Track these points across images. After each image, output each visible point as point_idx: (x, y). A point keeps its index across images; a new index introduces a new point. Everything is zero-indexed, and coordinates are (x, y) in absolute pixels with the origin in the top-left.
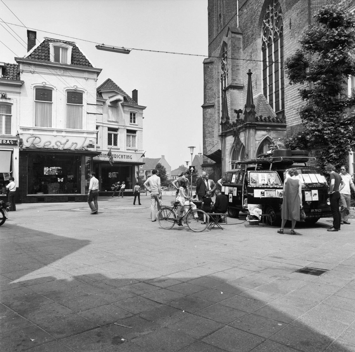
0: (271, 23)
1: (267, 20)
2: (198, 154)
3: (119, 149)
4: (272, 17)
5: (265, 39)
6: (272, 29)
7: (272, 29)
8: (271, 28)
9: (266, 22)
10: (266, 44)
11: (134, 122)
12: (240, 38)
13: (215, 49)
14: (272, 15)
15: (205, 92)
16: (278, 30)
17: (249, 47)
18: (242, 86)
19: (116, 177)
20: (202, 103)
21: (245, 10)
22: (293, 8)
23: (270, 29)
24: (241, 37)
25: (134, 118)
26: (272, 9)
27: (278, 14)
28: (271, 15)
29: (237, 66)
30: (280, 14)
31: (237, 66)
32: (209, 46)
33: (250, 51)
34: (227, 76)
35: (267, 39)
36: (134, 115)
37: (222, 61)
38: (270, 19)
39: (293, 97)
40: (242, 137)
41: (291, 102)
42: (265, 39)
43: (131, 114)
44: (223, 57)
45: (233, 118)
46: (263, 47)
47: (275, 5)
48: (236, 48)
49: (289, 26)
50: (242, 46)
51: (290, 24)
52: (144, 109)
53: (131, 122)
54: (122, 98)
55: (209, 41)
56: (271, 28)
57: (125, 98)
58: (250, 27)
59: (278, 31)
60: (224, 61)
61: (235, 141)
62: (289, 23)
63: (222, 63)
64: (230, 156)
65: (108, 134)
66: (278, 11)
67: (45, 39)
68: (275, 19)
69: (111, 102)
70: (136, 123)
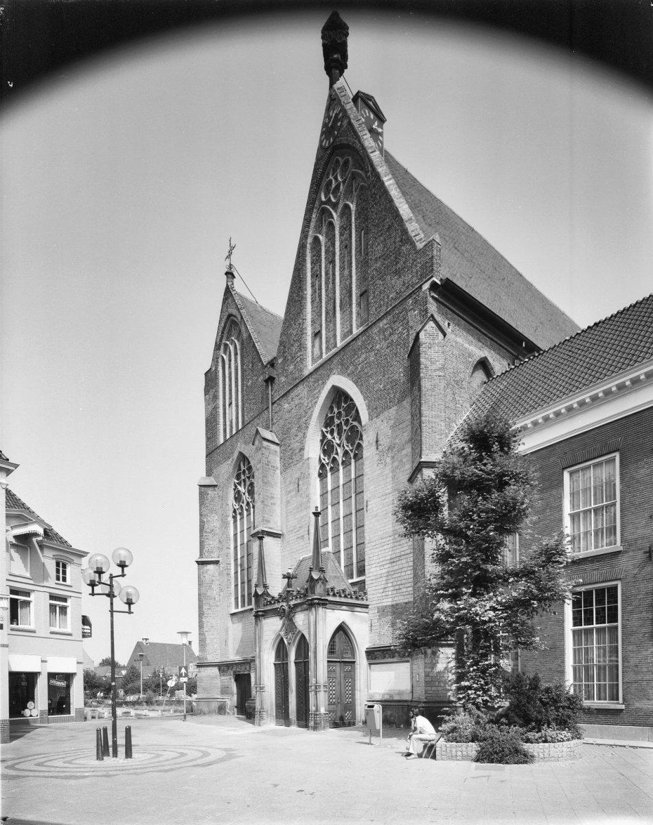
0: (335, 434)
1: (329, 429)
2: (141, 640)
3: (70, 635)
4: (339, 426)
5: (324, 459)
6: (339, 445)
7: (339, 445)
8: (337, 444)
9: (327, 432)
10: (328, 468)
11: (64, 579)
12: (276, 452)
13: (219, 463)
14: (339, 422)
15: (201, 536)
16: (351, 448)
17: (293, 468)
18: (280, 533)
19: (402, 726)
20: (197, 557)
21: (286, 406)
22: (382, 417)
23: (335, 444)
24: (277, 448)
25: (64, 573)
26: (339, 413)
27: (351, 422)
28: (337, 421)
29: (272, 498)
30: (355, 423)
31: (272, 498)
32: (207, 457)
33: (297, 476)
34: (252, 510)
35: (328, 459)
36: (64, 566)
37: (236, 486)
38: (335, 428)
39: (381, 560)
40: (300, 619)
41: (378, 569)
42: (324, 459)
43: (58, 564)
44: (238, 479)
45: (276, 587)
46: (321, 472)
47: (345, 406)
48: (270, 467)
49: (375, 444)
50: (278, 463)
51: (377, 441)
52: (83, 556)
53: (58, 579)
54: (41, 531)
55: (207, 447)
56: (337, 444)
57: (45, 531)
58: (296, 436)
59: (351, 450)
60: (239, 487)
61: (283, 626)
62: (375, 440)
63: (234, 490)
64: (274, 645)
65: (50, 605)
66: (351, 417)
67: (420, 246)
68: (345, 430)
69: (16, 537)
70: (68, 582)
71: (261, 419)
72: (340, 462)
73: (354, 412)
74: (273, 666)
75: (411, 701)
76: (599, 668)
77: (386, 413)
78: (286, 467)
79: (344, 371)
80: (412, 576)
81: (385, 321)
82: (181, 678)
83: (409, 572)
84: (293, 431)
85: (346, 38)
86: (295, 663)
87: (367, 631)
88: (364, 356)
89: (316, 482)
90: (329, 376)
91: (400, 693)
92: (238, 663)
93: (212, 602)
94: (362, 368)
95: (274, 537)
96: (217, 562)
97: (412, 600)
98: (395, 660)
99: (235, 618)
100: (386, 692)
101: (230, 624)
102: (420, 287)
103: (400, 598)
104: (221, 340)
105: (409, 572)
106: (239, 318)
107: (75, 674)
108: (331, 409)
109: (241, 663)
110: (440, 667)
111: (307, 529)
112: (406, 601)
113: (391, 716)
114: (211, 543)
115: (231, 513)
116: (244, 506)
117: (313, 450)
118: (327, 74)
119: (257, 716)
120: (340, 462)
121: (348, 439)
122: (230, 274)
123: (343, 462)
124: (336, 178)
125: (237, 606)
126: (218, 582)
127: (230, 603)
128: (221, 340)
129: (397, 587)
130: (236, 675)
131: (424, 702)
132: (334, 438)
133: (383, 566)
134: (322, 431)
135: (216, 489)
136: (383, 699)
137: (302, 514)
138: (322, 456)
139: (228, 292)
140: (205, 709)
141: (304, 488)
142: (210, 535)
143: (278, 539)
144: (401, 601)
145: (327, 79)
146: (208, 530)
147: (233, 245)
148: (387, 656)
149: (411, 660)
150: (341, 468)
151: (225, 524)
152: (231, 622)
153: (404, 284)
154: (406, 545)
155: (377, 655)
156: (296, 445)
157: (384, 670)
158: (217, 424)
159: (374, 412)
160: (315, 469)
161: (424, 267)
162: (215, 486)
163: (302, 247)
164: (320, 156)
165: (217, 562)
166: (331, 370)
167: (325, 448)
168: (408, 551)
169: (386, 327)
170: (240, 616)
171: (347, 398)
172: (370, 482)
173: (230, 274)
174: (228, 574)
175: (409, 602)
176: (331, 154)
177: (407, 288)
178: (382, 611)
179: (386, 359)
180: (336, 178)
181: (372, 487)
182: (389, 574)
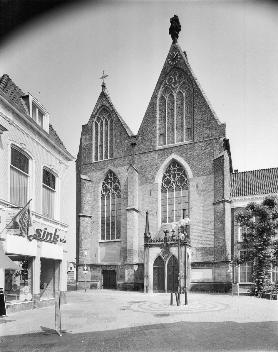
5: (165, 186)
6: (110, 189)
22: (199, 178)
33: (151, 188)
47: (178, 168)
49: (196, 186)
51: (197, 186)
68: (177, 177)
71: (126, 159)
72: (174, 189)
73: (183, 171)
74: (153, 268)
75: (214, 283)
76: (248, 273)
77: (202, 177)
78: (142, 183)
79: (180, 154)
80: (213, 238)
81: (202, 144)
82: (84, 272)
83: (212, 236)
84: (148, 170)
85: (178, 32)
86: (167, 267)
87: (192, 254)
88: (191, 152)
89: (160, 195)
90: (171, 154)
91: (208, 280)
92: (106, 265)
93: (87, 235)
94: (190, 156)
95: (137, 212)
96: (90, 217)
97: (213, 246)
98: (205, 267)
99: (102, 245)
100: (201, 279)
101: (99, 247)
102: (219, 138)
103: (207, 245)
104: (96, 114)
105: (212, 236)
106: (111, 110)
107: (61, 260)
108: (170, 167)
109: (108, 265)
110: (229, 271)
111: (156, 212)
112: (211, 246)
113: (204, 288)
114: (193, 198)
115: (100, 195)
116: (111, 194)
117: (159, 180)
118: (172, 39)
119: (145, 288)
120: (174, 189)
121: (114, 188)
122: (103, 86)
123: (175, 189)
124: (175, 79)
125: (103, 238)
126: (90, 226)
127: (99, 237)
128: (96, 114)
129: (206, 241)
130: (104, 271)
131: (226, 283)
132: (171, 178)
133: (199, 232)
134: (164, 174)
135: (90, 182)
136: (199, 282)
137: (153, 205)
138: (163, 184)
139: (103, 95)
140: (83, 286)
141: (154, 195)
142: (87, 203)
143: (137, 213)
144: (208, 246)
145: (172, 41)
146: (86, 201)
147: (106, 74)
148: (201, 266)
149: (213, 268)
150: (174, 191)
151: (96, 199)
152: (99, 246)
153: (212, 134)
154: (210, 226)
155: (194, 265)
156: (149, 176)
157: (199, 271)
158: (91, 152)
159: (196, 175)
160: (160, 189)
161: (221, 132)
162: (91, 181)
163: (154, 97)
164: (165, 66)
165: (90, 217)
166: (172, 152)
167: (166, 181)
168: (212, 229)
169: (203, 146)
170: (107, 243)
171: (179, 164)
172: (193, 200)
173: (103, 86)
174: (98, 224)
175: (212, 247)
176: (173, 69)
177: (213, 136)
178: (198, 249)
179: (203, 157)
180: (175, 79)
181: (194, 202)
182: (201, 236)
